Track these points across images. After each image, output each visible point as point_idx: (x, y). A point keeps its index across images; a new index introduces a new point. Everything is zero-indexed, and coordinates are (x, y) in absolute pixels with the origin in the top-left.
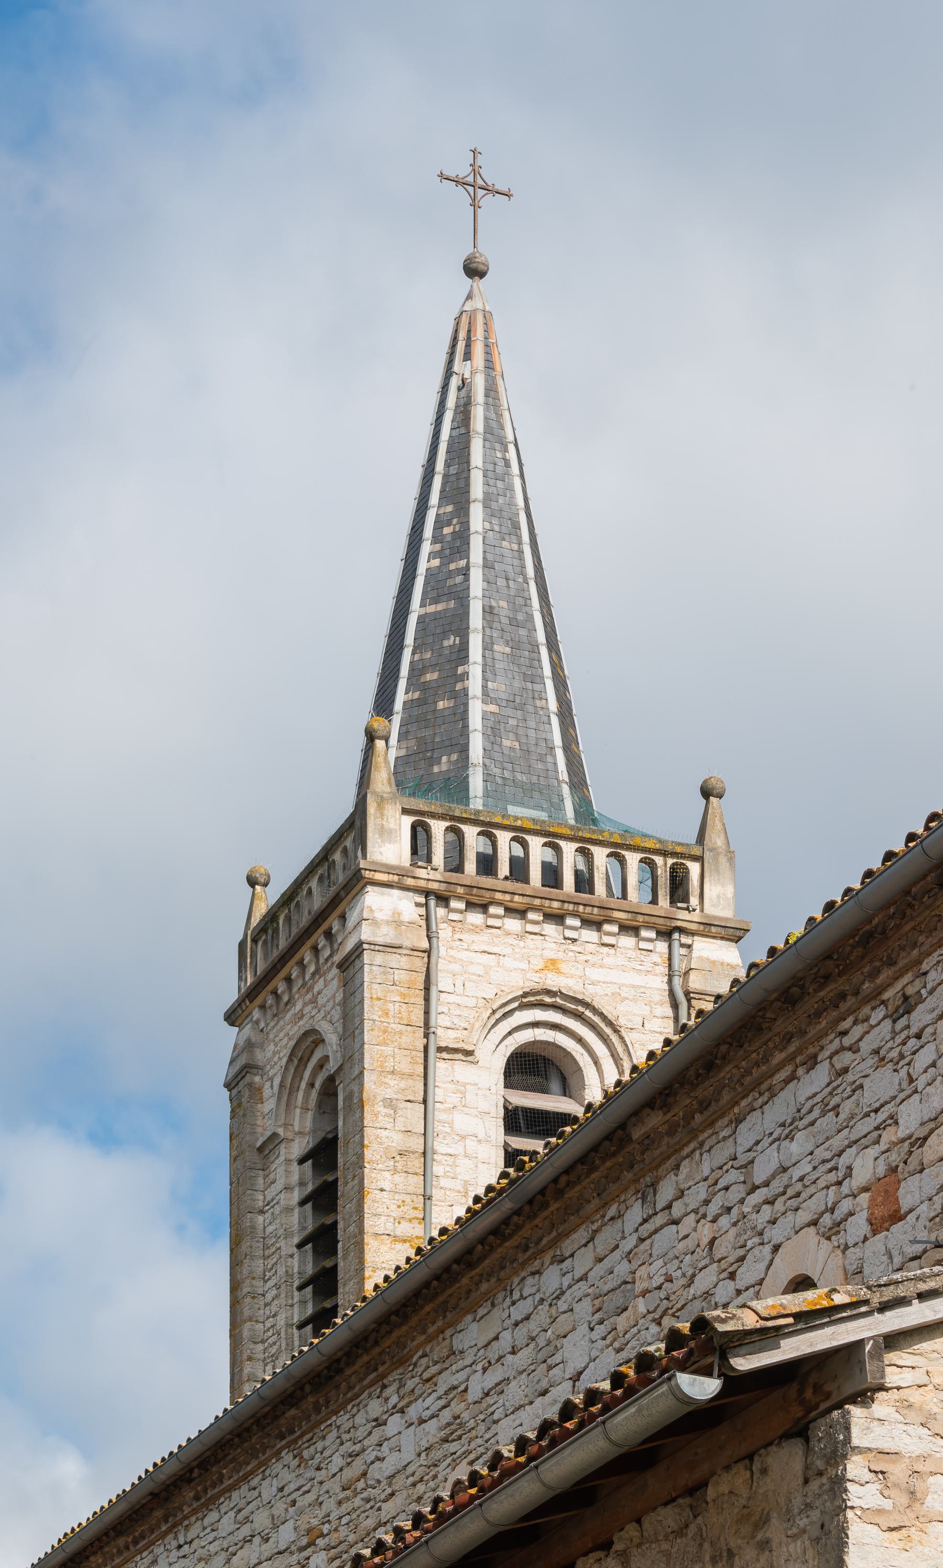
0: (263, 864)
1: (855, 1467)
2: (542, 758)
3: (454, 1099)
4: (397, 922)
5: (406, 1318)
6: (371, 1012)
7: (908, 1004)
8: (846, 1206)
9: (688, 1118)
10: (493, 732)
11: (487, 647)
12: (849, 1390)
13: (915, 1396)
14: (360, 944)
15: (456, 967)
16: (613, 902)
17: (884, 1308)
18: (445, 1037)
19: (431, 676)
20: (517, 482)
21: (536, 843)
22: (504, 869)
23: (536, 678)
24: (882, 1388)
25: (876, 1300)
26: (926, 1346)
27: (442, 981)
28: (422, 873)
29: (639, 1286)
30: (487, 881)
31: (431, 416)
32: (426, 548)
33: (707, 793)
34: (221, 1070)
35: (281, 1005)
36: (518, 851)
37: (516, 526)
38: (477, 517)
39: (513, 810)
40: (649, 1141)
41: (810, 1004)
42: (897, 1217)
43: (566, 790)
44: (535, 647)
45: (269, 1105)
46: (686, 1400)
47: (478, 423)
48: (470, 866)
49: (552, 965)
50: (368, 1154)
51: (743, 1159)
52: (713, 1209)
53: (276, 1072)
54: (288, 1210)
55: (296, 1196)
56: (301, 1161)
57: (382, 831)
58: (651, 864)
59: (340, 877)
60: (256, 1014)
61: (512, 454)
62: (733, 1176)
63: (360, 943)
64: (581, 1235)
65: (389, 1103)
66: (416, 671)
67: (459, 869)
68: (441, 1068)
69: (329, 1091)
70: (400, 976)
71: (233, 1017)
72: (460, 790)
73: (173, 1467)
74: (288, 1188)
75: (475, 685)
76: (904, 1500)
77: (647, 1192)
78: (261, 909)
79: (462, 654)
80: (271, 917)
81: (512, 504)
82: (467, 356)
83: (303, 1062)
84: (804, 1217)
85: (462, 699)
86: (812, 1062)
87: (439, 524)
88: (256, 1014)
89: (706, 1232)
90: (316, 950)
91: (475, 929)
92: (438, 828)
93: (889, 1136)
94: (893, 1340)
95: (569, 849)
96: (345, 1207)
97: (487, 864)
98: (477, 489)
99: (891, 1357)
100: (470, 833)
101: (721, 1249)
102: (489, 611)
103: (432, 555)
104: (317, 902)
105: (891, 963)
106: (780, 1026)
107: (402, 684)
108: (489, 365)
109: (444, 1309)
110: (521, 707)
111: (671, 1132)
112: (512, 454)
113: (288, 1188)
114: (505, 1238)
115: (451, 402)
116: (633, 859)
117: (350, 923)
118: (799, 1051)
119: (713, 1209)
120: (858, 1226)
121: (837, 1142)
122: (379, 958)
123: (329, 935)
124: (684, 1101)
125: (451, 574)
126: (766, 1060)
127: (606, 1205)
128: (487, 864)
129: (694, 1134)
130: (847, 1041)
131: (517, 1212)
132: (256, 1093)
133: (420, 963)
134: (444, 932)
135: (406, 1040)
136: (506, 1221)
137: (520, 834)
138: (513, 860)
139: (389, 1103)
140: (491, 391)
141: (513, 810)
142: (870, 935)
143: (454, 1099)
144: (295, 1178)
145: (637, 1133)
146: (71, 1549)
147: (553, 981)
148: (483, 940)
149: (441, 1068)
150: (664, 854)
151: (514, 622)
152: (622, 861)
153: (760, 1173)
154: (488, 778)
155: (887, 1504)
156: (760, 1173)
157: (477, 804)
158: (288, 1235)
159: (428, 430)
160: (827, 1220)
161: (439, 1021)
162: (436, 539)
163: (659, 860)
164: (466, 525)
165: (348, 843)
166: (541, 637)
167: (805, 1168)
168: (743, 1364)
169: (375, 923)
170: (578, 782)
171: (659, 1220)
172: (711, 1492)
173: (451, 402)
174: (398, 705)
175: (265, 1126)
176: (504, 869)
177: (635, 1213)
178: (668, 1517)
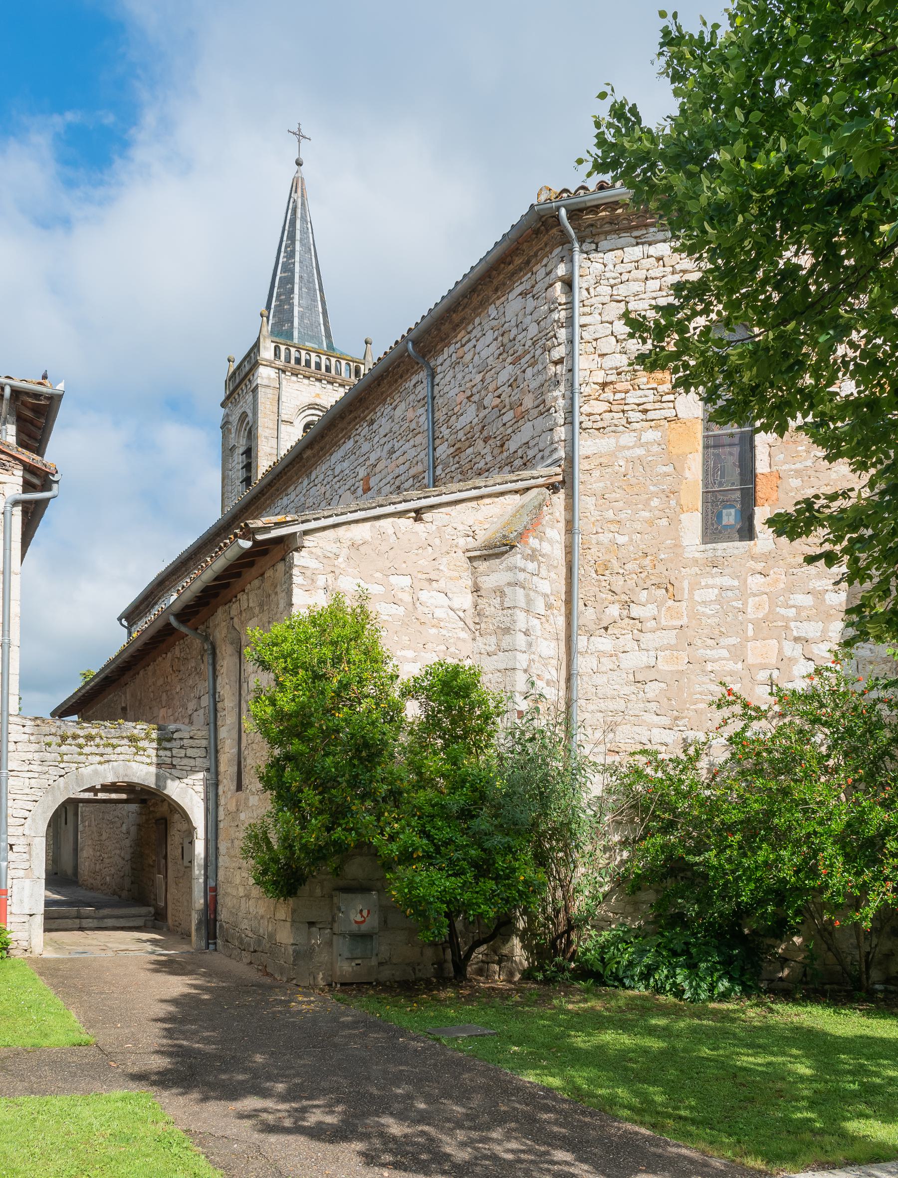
0: (232, 356)
1: (295, 571)
2: (316, 327)
3: (287, 438)
4: (269, 378)
5: (247, 510)
6: (261, 407)
7: (372, 422)
8: (357, 485)
9: (318, 452)
10: (301, 317)
11: (300, 289)
12: (294, 547)
13: (314, 550)
14: (257, 385)
15: (288, 394)
16: (337, 376)
17: (303, 522)
18: (284, 417)
19: (283, 297)
20: (311, 235)
21: (313, 355)
22: (303, 363)
23: (315, 301)
24: (303, 547)
25: (300, 520)
26: (317, 535)
27: (283, 399)
28: (277, 362)
29: (307, 505)
30: (297, 367)
31: (285, 211)
32: (282, 254)
33: (366, 343)
34: (219, 423)
35: (236, 403)
36: (308, 357)
37: (310, 250)
38: (298, 244)
39: (307, 344)
40: (308, 459)
41: (347, 420)
42: (369, 489)
43: (324, 338)
44: (315, 291)
45: (233, 435)
46: (242, 548)
47: (299, 215)
48: (293, 361)
49: (318, 395)
50: (259, 454)
51: (332, 467)
52: (325, 482)
53: (235, 424)
54: (238, 470)
55: (241, 466)
56: (242, 454)
57: (265, 347)
58: (349, 365)
59: (253, 361)
60: (230, 405)
61: (309, 226)
62: (330, 472)
63: (257, 385)
64: (292, 488)
65: (266, 437)
66: (278, 295)
67: (289, 362)
68: (283, 427)
69: (250, 432)
70: (270, 396)
71: (223, 405)
72: (290, 336)
73: (186, 554)
74: (238, 463)
75: (296, 301)
76: (310, 582)
77: (309, 476)
78: (232, 370)
79: (292, 291)
80: (234, 373)
81: (309, 242)
82: (296, 192)
83: (243, 422)
84: (347, 487)
85: (292, 305)
86: (349, 438)
87: (286, 247)
88: (230, 405)
89: (323, 490)
90: (246, 386)
91: (294, 382)
92: (283, 348)
93: (368, 463)
94: (306, 533)
95: (324, 358)
96: (253, 471)
97: (298, 361)
98: (298, 236)
99: (307, 537)
100: (293, 350)
101: (327, 495)
102: (301, 277)
103: (284, 257)
104: (247, 369)
105: (368, 408)
106: (340, 425)
107: (274, 299)
108: (303, 196)
109: (257, 508)
110: (310, 310)
111: (314, 457)
112: (309, 226)
113: (238, 463)
114: (272, 487)
115: (291, 207)
116: (343, 362)
117: (255, 377)
118: (346, 434)
119: (325, 482)
120: (360, 491)
121: (355, 464)
122: (263, 390)
123: (249, 380)
124: (317, 447)
125: (289, 264)
126: (337, 436)
127: (298, 478)
128: (298, 361)
129: (320, 458)
130: (358, 432)
131: (275, 479)
132: (229, 431)
133: (276, 392)
134: (284, 382)
135: (271, 417)
136: (272, 481)
137: (308, 351)
138: (306, 360)
139: (266, 437)
140: (303, 204)
141: (307, 344)
142: (361, 399)
143: (287, 438)
144: (240, 460)
145: (305, 456)
146: (159, 579)
147: (318, 401)
148: (296, 386)
149: (283, 427)
150: (353, 362)
151: (309, 282)
152: (340, 363)
153: (337, 472)
154: (299, 332)
155: (305, 583)
156: (337, 472)
157: (296, 341)
158: (238, 478)
159: (284, 215)
160: (352, 489)
161: (282, 412)
162: (285, 252)
163: (351, 363)
164: (294, 248)
165: (256, 350)
166: (317, 287)
167: (347, 472)
168: (259, 537)
169: (262, 378)
170: (328, 336)
171: (311, 485)
172: (266, 576)
173: (291, 207)
174: (273, 306)
175: (232, 442)
176: (303, 363)
177: (306, 482)
178: (256, 583)
